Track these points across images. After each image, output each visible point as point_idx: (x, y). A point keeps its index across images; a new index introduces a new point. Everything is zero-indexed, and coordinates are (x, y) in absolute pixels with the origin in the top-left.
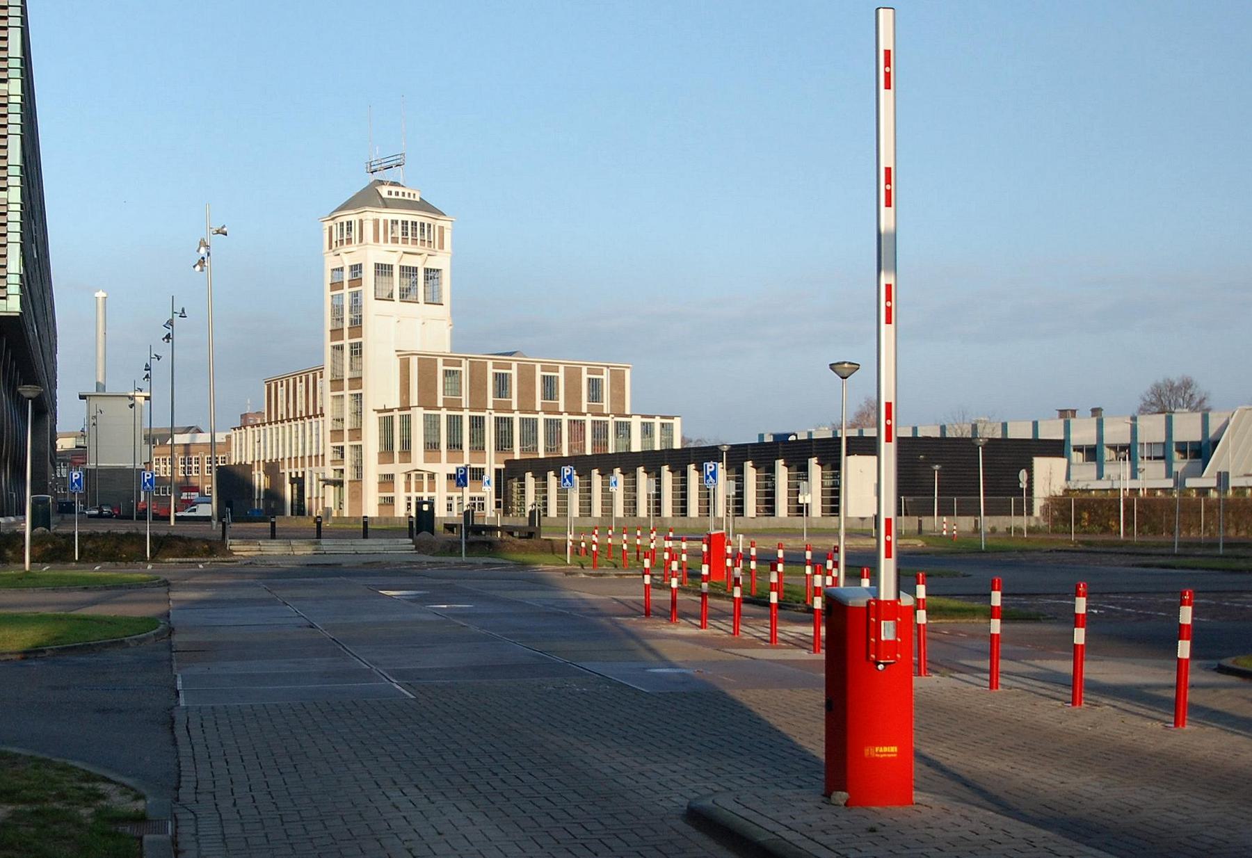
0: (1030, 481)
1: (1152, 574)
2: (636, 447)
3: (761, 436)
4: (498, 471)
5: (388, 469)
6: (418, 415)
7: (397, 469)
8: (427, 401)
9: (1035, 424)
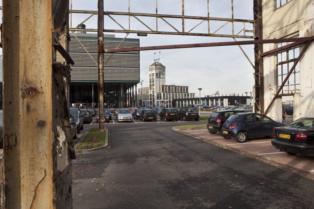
0: (228, 103)
1: (170, 123)
2: (190, 97)
3: (205, 96)
4: (172, 101)
5: (158, 101)
6: (162, 93)
7: (159, 100)
8: (163, 91)
9: (243, 94)
